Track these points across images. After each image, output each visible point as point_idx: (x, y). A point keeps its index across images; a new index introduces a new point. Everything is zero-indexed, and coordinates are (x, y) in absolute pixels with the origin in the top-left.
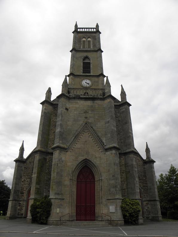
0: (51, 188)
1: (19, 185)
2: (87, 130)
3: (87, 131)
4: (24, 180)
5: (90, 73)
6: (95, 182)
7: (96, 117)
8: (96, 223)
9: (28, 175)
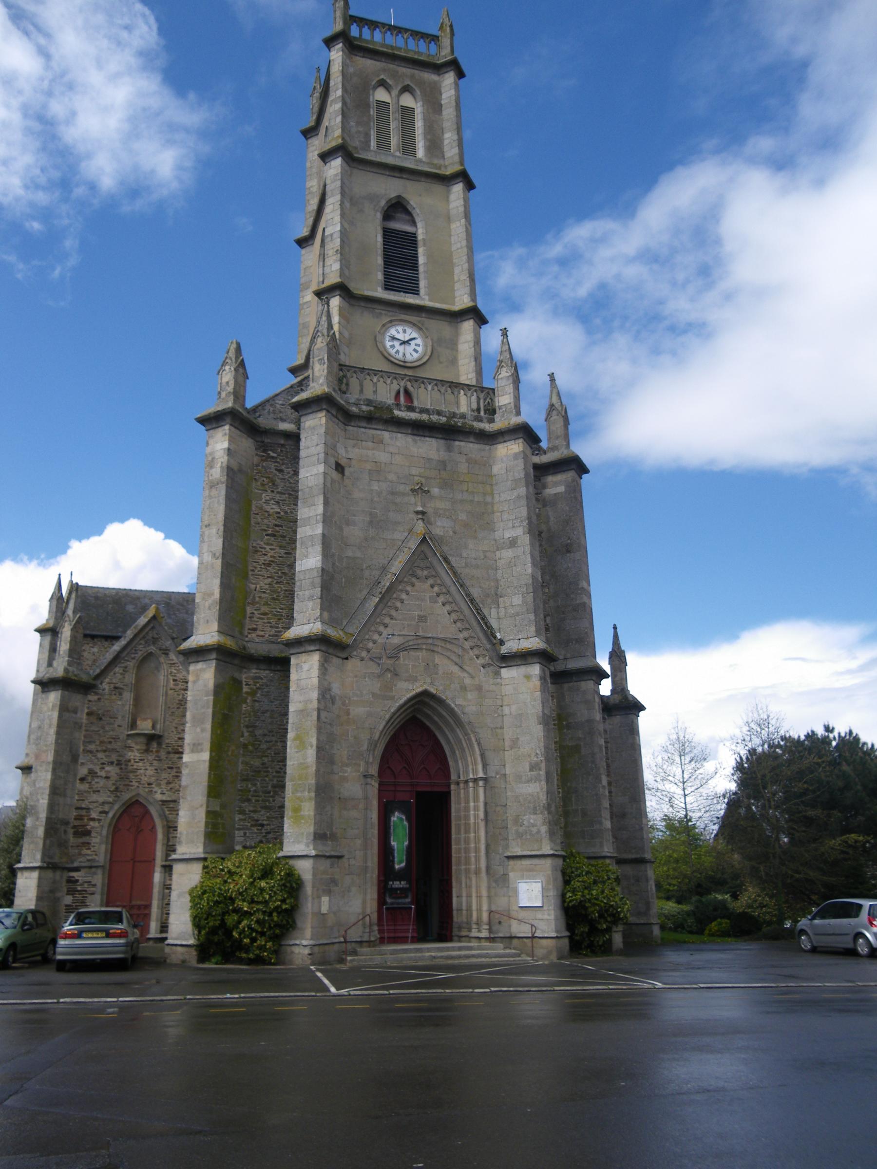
0: (288, 813)
1: (65, 796)
2: (428, 568)
3: (425, 573)
4: (91, 772)
5: (416, 292)
6: (453, 787)
7: (463, 516)
8: (471, 948)
9: (109, 746)
